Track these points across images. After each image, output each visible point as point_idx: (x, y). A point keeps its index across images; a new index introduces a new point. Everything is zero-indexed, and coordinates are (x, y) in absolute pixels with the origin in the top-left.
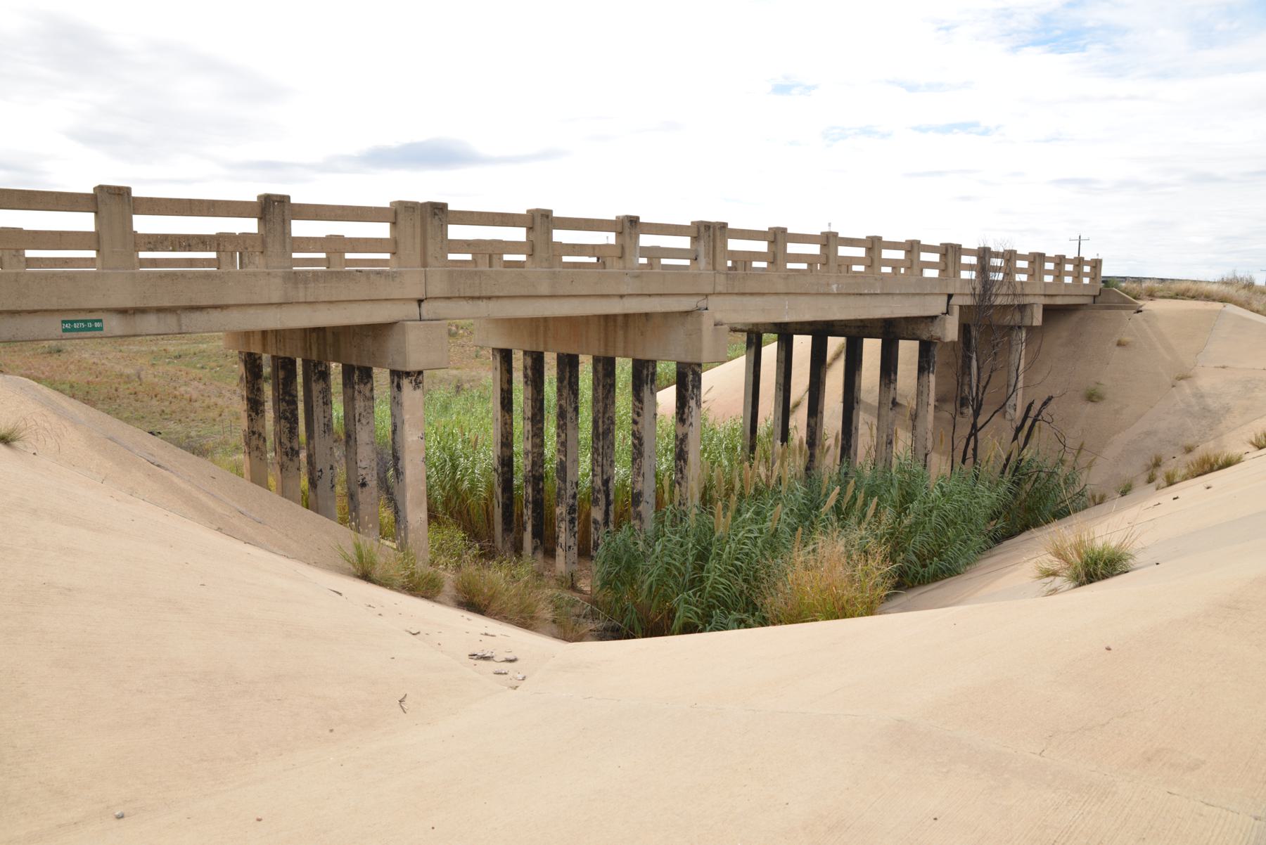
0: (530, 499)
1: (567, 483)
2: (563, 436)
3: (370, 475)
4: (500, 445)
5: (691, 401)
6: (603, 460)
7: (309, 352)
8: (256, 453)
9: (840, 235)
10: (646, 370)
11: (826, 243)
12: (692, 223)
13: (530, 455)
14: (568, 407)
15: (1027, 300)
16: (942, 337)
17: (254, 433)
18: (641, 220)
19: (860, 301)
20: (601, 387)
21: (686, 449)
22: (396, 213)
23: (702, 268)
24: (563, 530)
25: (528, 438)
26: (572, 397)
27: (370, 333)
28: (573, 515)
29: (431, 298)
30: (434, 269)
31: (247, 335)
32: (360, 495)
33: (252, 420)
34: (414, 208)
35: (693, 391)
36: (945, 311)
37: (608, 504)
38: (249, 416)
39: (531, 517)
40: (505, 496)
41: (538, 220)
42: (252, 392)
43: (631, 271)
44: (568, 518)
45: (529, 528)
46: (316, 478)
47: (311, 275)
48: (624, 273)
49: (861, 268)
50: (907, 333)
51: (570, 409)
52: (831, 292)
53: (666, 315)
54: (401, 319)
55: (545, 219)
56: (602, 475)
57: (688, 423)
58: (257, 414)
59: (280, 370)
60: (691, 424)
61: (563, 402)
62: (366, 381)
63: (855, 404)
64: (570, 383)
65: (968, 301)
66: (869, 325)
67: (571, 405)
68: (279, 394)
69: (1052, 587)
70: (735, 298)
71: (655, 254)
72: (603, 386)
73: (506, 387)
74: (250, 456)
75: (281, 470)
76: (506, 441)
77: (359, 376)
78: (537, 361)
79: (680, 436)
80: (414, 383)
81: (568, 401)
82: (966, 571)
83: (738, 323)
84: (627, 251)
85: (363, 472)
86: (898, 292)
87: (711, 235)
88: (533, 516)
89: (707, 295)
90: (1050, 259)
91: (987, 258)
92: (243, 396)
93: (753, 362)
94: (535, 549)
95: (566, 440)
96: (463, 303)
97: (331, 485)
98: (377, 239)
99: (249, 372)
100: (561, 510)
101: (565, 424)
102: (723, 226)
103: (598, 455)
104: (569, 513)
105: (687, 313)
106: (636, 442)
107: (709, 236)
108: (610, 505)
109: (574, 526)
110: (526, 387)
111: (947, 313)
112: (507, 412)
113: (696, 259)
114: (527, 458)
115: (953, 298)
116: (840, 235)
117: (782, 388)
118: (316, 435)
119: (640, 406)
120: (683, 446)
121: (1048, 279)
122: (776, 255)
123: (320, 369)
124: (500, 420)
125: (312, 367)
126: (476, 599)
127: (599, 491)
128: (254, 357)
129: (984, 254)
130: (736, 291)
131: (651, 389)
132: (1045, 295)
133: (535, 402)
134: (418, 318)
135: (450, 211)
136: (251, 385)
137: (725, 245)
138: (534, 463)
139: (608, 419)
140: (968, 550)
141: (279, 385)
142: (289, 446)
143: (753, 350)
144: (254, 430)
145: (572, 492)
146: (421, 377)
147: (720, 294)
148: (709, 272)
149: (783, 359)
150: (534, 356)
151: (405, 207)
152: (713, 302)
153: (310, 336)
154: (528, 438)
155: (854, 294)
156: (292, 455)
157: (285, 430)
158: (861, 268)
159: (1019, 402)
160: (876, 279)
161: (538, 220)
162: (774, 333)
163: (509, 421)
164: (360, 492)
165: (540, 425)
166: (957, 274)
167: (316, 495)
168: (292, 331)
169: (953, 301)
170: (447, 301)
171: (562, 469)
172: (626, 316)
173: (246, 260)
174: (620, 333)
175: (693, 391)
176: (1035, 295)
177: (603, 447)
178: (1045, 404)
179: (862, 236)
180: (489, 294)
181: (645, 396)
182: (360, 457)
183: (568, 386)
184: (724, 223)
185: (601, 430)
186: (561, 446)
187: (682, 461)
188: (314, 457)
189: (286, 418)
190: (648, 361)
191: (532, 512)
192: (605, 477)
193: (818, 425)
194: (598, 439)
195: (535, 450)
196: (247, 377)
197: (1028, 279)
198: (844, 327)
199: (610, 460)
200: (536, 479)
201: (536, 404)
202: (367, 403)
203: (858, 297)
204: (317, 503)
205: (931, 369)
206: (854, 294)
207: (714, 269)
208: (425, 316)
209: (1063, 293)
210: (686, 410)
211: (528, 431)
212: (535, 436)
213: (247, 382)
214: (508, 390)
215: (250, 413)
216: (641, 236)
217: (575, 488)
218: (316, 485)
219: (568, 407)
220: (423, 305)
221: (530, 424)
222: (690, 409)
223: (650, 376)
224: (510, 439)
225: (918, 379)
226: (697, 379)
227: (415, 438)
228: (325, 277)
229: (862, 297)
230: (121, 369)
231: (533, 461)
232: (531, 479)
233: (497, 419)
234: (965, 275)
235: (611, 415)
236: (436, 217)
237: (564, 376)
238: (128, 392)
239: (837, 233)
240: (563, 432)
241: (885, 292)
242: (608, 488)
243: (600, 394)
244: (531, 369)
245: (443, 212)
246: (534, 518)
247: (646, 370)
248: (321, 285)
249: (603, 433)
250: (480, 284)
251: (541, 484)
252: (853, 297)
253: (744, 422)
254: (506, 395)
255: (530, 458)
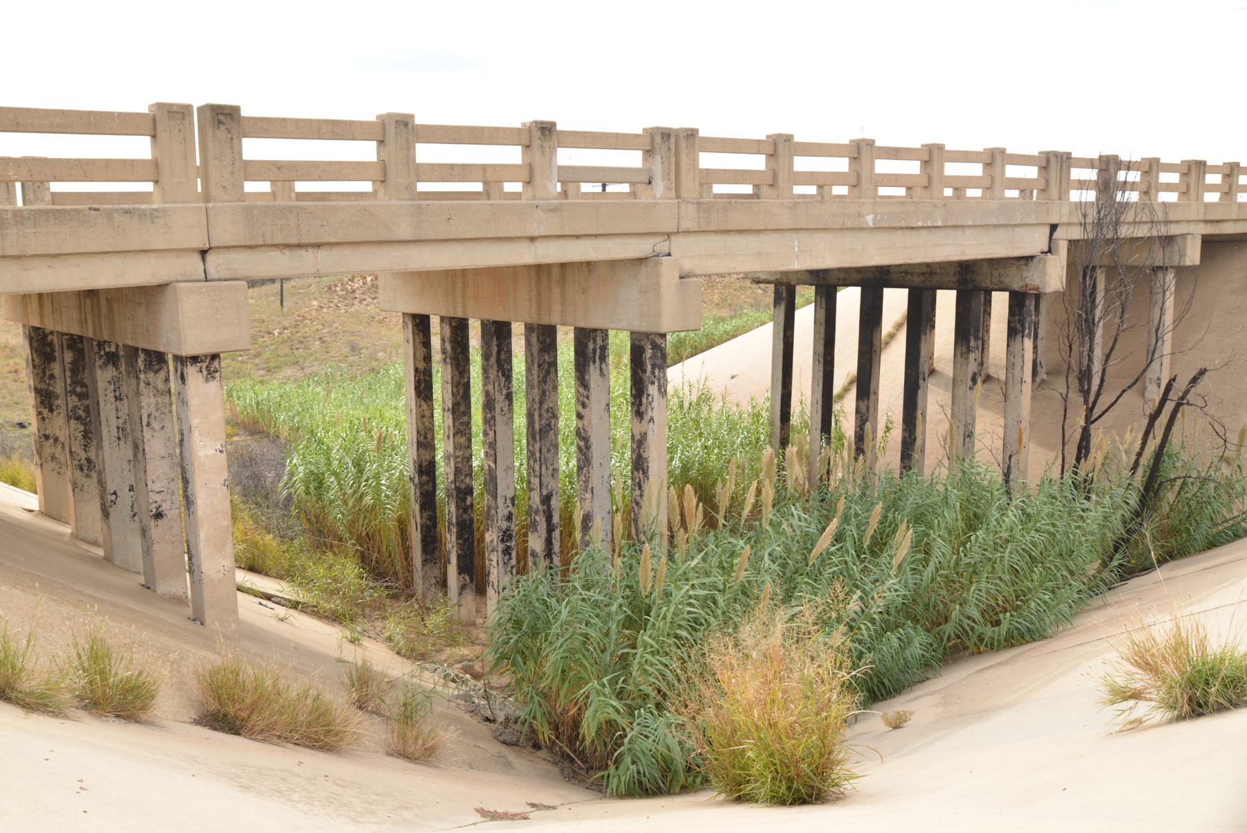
0: (454, 520)
1: (498, 499)
2: (491, 433)
3: (168, 502)
4: (415, 445)
5: (650, 387)
6: (540, 468)
7: (85, 326)
8: (51, 465)
9: (877, 144)
10: (591, 342)
11: (856, 156)
12: (645, 130)
13: (452, 459)
14: (497, 393)
15: (1174, 230)
16: (1041, 286)
17: (47, 437)
18: (559, 128)
19: (899, 238)
20: (536, 366)
21: (645, 455)
22: (154, 121)
23: (658, 196)
24: (494, 563)
25: (449, 437)
26: (503, 380)
27: (143, 301)
28: (508, 544)
29: (218, 248)
30: (221, 204)
31: (45, 300)
32: (153, 531)
33: (43, 419)
34: (183, 113)
35: (653, 373)
36: (1046, 249)
37: (550, 529)
38: (40, 413)
39: (455, 545)
40: (425, 515)
41: (391, 130)
42: (42, 381)
43: (542, 202)
44: (501, 547)
45: (454, 560)
46: (108, 504)
47: (10, 215)
48: (533, 205)
49: (840, 190)
50: (991, 281)
51: (500, 398)
52: (864, 225)
53: (614, 264)
54: (173, 279)
55: (403, 128)
56: (541, 489)
57: (647, 418)
58: (51, 410)
59: (65, 351)
60: (652, 420)
61: (490, 387)
62: (157, 367)
63: (921, 382)
64: (498, 361)
65: (1077, 234)
66: (938, 271)
67: (500, 391)
68: (66, 384)
69: (1132, 717)
70: (714, 237)
71: (572, 176)
72: (539, 366)
73: (421, 366)
74: (42, 469)
75: (74, 490)
76: (425, 442)
77: (145, 360)
78: (459, 329)
79: (638, 437)
80: (205, 373)
81: (496, 385)
82: (1056, 634)
83: (761, 272)
84: (537, 173)
85: (158, 498)
86: (970, 223)
87: (673, 147)
88: (458, 544)
89: (669, 235)
90: (1215, 169)
91: (1112, 170)
92: (30, 386)
93: (782, 324)
94: (463, 588)
95: (495, 440)
96: (275, 254)
97: (132, 514)
98: (125, 161)
99: (36, 352)
100: (491, 537)
101: (494, 418)
102: (692, 134)
103: (535, 461)
104: (502, 541)
105: (640, 261)
106: (582, 443)
107: (669, 149)
108: (554, 530)
109: (510, 559)
110: (444, 366)
111: (1050, 251)
112: (425, 401)
113: (650, 183)
114: (448, 464)
115: (1058, 229)
116: (877, 144)
117: (822, 360)
118: (106, 444)
119: (585, 393)
120: (642, 451)
121: (1212, 197)
122: (859, 179)
123: (107, 350)
124: (414, 411)
125: (96, 348)
126: (231, 710)
127: (537, 512)
128: (44, 332)
129: (1108, 165)
130: (713, 227)
131: (601, 370)
132: (1206, 222)
133: (457, 387)
134: (203, 276)
135: (243, 117)
136: (40, 371)
137: (695, 161)
138: (457, 471)
139: (547, 411)
140: (1058, 604)
141: (65, 371)
142: (83, 456)
143: (782, 308)
144: (47, 433)
145: (506, 512)
146: (216, 363)
147: (688, 232)
148: (670, 201)
149: (823, 321)
150: (454, 324)
151: (169, 112)
152: (679, 245)
153: (85, 304)
154: (449, 437)
155: (902, 228)
156: (89, 469)
157: (77, 434)
158: (840, 190)
159: (1162, 370)
160: (935, 206)
161: (391, 130)
162: (811, 285)
163: (427, 413)
164: (153, 527)
165: (465, 419)
166: (1063, 195)
167: (109, 528)
168: (66, 294)
169: (1059, 234)
170: (249, 251)
171: (491, 480)
172: (563, 266)
173: (31, 196)
174: (556, 291)
175: (653, 373)
176: (1189, 221)
177: (540, 450)
178: (1194, 380)
179: (979, 147)
180: (313, 240)
181: (592, 379)
182: (151, 475)
183: (496, 366)
184: (692, 130)
185: (537, 427)
186: (489, 448)
187: (641, 472)
188: (103, 475)
189: (78, 418)
190: (595, 330)
191: (458, 538)
192: (545, 492)
193: (871, 409)
194: (534, 439)
195: (459, 453)
196: (33, 360)
197: (849, 192)
198: (903, 275)
199: (551, 468)
200: (463, 493)
201: (458, 391)
202: (160, 400)
203: (908, 232)
204: (111, 539)
205: (1027, 331)
206: (902, 228)
207: (678, 197)
208: (212, 273)
209: (1235, 217)
210: (644, 400)
211: (449, 427)
212: (457, 433)
213: (34, 367)
214: (425, 369)
215: (40, 410)
216: (560, 150)
217: (510, 505)
218: (109, 514)
219: (497, 393)
220: (209, 257)
221: (451, 417)
222: (650, 399)
223: (598, 351)
224: (429, 436)
225: (1008, 346)
226: (659, 355)
227: (211, 452)
228: (35, 217)
229: (914, 233)
230: (7, 340)
231: (456, 468)
232: (454, 493)
233: (411, 411)
234: (1075, 196)
235: (551, 405)
236: (222, 128)
237: (491, 351)
238: (8, 368)
239: (873, 141)
240: (491, 430)
241: (950, 224)
242: (549, 506)
243: (535, 377)
244: (450, 342)
245: (232, 119)
246: (461, 547)
247: (591, 342)
248: (28, 231)
249: (540, 430)
250: (299, 225)
251: (469, 498)
252: (900, 232)
253: (772, 406)
254: (422, 377)
255: (452, 464)
